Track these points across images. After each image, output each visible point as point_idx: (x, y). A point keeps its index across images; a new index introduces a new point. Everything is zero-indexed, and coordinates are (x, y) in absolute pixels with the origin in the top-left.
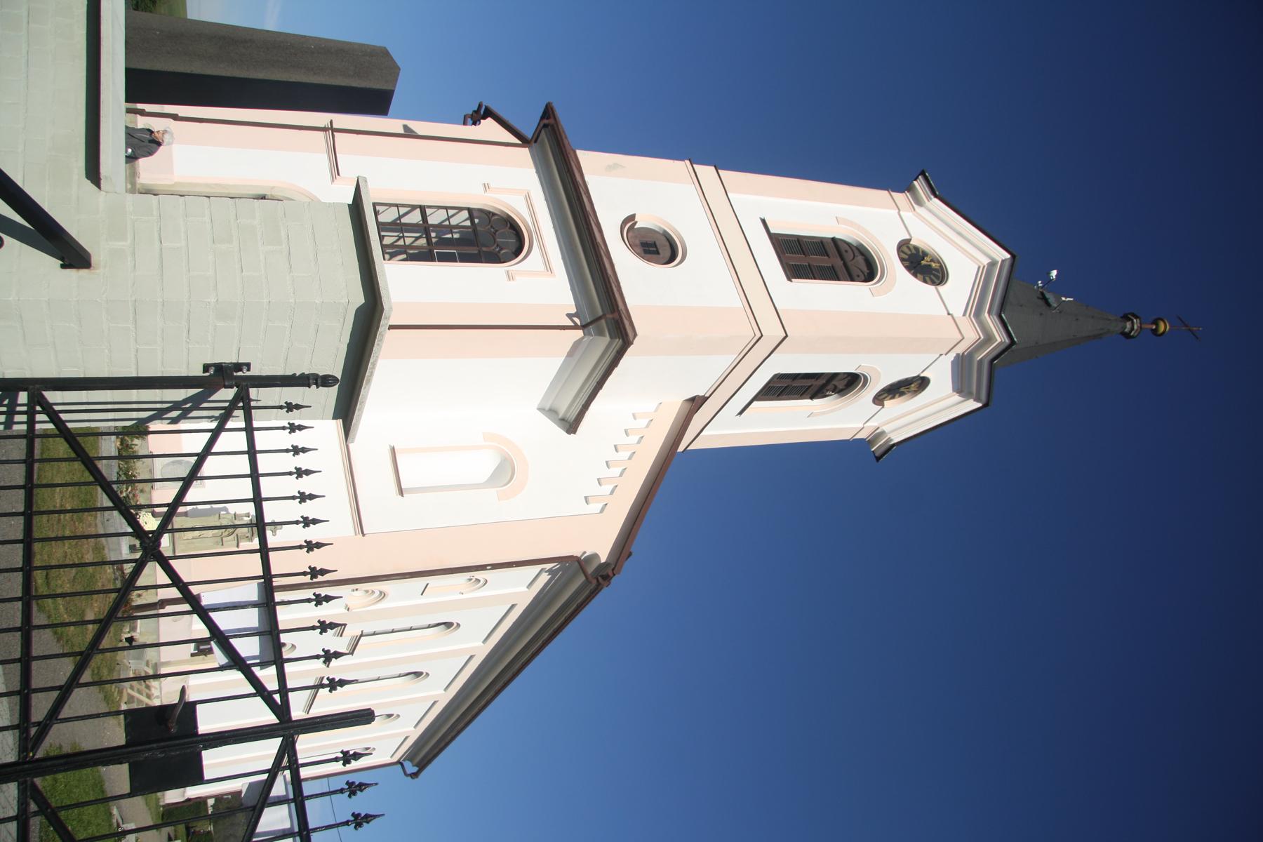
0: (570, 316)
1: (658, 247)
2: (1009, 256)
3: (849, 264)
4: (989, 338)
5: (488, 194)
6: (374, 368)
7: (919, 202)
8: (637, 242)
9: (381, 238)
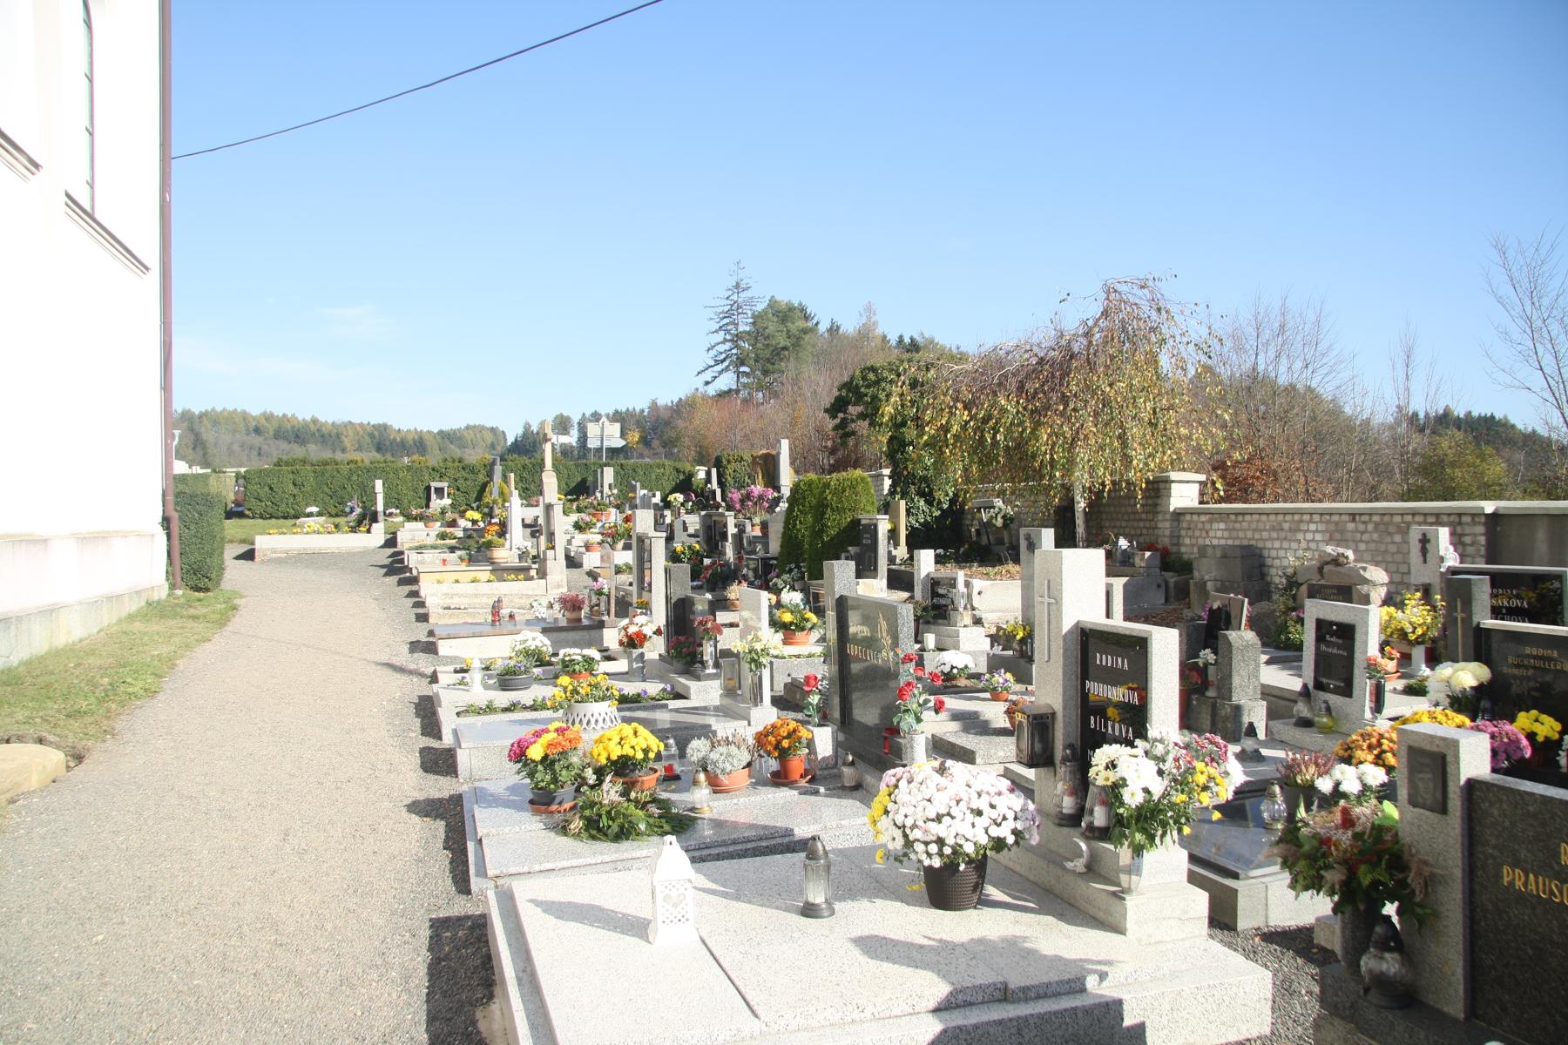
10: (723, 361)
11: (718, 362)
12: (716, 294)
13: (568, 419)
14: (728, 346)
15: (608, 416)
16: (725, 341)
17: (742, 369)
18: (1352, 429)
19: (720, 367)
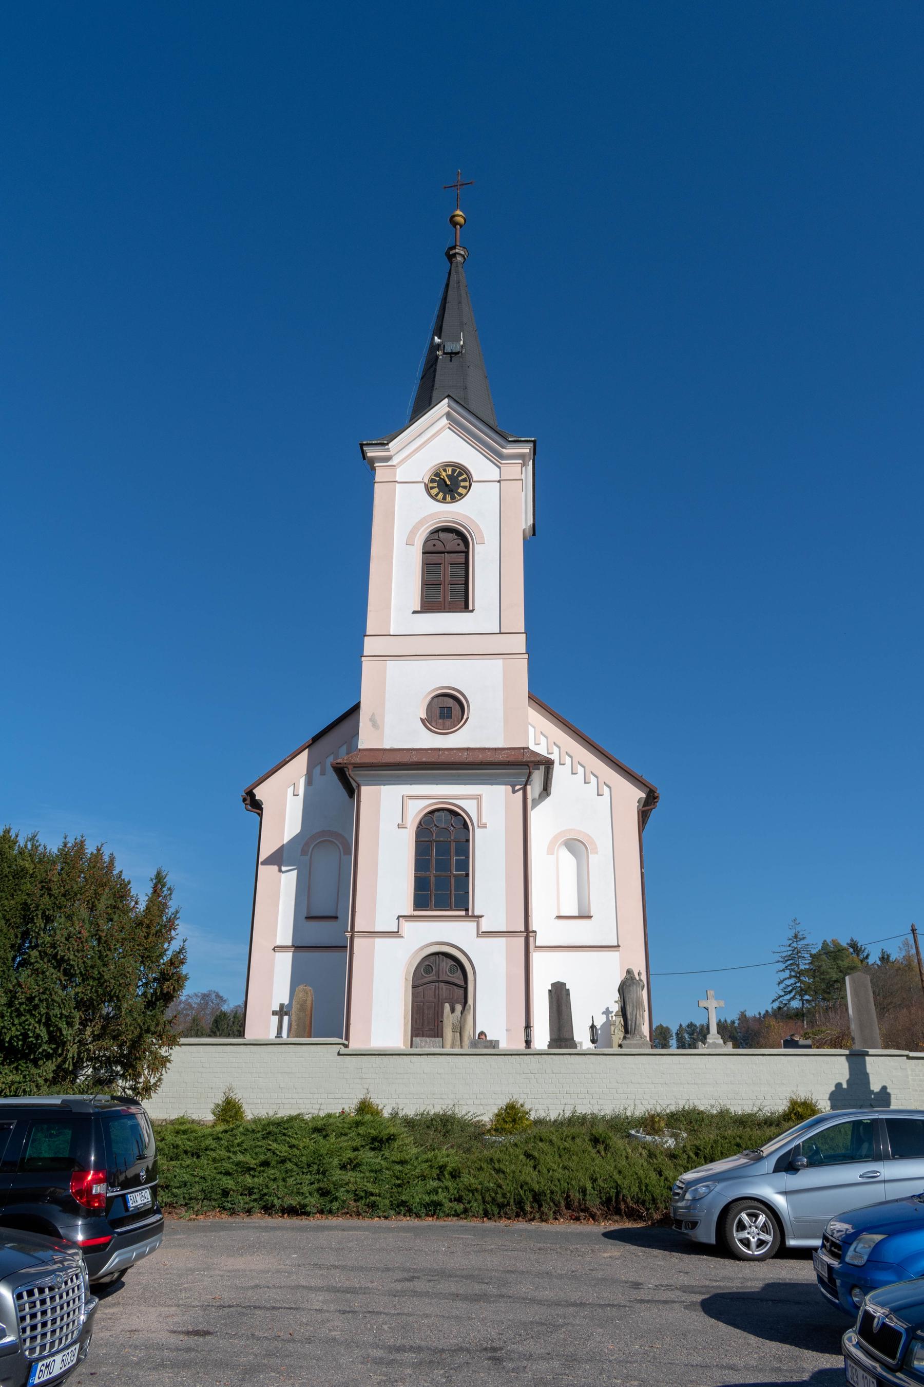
0: (514, 792)
1: (447, 709)
2: (446, 400)
3: (448, 549)
4: (522, 456)
5: (409, 826)
6: (405, 1031)
7: (388, 459)
8: (440, 721)
9: (6, 1096)
10: (790, 992)
11: (787, 993)
12: (780, 943)
13: (667, 1029)
14: (792, 981)
15: (723, 1028)
16: (791, 977)
17: (807, 997)
18: (646, 1120)
19: (788, 997)
